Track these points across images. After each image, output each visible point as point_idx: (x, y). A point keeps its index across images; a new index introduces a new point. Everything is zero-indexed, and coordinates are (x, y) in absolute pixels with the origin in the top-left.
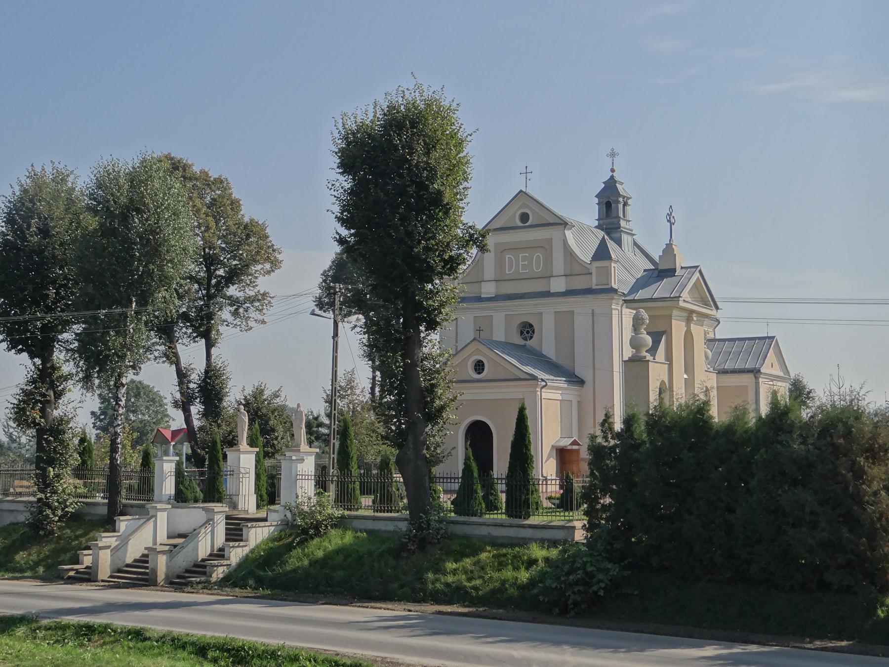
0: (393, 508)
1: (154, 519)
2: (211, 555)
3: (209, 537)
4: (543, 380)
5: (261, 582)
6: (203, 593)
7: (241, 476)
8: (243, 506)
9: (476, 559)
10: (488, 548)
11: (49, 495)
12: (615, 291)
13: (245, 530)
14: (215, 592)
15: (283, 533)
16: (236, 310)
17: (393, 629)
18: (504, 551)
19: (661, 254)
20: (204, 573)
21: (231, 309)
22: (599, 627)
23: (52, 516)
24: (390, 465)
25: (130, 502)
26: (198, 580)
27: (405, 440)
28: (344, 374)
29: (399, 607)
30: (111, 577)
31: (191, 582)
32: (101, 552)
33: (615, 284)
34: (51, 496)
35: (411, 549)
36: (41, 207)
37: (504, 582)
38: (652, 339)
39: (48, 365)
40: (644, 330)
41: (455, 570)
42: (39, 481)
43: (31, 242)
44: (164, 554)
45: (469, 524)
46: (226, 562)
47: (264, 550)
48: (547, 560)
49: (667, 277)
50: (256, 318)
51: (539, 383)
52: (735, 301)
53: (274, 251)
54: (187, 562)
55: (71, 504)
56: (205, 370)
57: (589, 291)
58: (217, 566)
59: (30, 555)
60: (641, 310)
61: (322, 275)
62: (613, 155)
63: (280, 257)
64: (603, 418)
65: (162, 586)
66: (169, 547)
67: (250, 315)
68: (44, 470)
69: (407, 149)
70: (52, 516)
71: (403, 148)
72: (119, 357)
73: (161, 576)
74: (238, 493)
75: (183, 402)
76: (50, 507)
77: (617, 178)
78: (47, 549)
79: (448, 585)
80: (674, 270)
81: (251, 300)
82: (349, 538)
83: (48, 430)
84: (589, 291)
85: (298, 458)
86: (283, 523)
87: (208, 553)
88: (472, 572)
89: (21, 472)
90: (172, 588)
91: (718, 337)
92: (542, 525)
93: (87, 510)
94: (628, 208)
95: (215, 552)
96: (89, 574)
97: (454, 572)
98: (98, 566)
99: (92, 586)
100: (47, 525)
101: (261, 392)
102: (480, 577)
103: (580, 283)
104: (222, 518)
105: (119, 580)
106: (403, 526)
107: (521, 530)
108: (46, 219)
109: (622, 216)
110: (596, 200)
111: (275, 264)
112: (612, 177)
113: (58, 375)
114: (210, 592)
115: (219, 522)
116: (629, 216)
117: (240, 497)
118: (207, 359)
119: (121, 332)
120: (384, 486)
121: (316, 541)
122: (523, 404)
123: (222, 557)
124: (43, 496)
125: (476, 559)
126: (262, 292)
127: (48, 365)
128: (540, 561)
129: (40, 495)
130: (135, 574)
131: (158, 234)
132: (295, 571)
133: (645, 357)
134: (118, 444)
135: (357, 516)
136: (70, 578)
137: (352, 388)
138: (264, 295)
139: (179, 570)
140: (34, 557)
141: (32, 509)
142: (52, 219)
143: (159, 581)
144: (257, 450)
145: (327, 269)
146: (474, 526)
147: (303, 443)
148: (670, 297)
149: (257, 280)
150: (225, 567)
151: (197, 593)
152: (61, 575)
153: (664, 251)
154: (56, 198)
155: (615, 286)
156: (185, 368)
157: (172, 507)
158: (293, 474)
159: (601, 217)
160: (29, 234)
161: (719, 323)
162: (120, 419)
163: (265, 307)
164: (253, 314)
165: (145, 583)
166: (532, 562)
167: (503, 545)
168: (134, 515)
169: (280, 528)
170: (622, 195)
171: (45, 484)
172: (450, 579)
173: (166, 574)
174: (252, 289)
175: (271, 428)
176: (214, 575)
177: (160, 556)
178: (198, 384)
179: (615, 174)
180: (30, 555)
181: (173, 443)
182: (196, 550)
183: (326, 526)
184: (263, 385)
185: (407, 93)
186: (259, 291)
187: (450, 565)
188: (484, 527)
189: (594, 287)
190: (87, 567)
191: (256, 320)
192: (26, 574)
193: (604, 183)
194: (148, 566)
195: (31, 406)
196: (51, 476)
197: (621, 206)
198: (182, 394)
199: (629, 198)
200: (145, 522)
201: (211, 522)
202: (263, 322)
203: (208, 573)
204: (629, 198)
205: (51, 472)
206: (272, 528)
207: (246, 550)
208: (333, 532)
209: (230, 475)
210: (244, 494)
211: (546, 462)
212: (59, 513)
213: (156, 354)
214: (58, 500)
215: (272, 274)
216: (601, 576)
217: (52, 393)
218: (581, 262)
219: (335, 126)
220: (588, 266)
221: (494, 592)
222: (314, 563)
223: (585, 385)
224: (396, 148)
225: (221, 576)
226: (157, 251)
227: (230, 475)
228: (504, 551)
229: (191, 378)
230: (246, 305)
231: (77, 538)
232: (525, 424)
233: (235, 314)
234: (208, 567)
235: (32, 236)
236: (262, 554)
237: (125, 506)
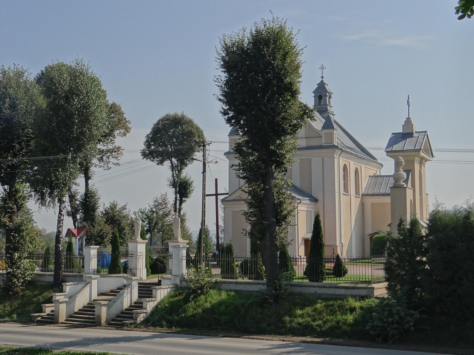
0: (235, 276)
1: (90, 284)
2: (130, 306)
3: (129, 295)
4: (299, 199)
5: (170, 324)
6: (136, 331)
7: (138, 257)
9: (313, 307)
10: (320, 301)
11: (15, 269)
12: (337, 147)
13: (154, 291)
14: (143, 330)
15: (177, 292)
16: (102, 157)
18: (331, 303)
19: (404, 124)
20: (132, 318)
21: (98, 156)
22: (385, 348)
23: (17, 283)
24: (232, 250)
25: (67, 273)
26: (130, 322)
27: (264, 235)
28: (161, 196)
29: (275, 338)
30: (66, 320)
32: (61, 305)
33: (335, 143)
34: (16, 271)
35: (270, 302)
36: (11, 91)
37: (338, 322)
38: (407, 174)
39: (13, 190)
40: (402, 169)
41: (302, 315)
42: (8, 261)
43: (6, 114)
44: (105, 306)
45: (301, 286)
46: (145, 311)
47: (168, 303)
48: (361, 308)
49: (409, 137)
50: (113, 162)
51: (297, 201)
52: (441, 150)
53: (126, 122)
54: (117, 310)
55: (28, 275)
56: (85, 193)
57: (320, 147)
58: (140, 313)
59: (5, 307)
60: (400, 157)
62: (322, 68)
63: (130, 126)
64: (399, 222)
65: (104, 326)
66: (108, 302)
67: (110, 160)
68: (12, 254)
69: (272, 57)
70: (17, 283)
71: (269, 56)
72: (64, 184)
73: (103, 320)
74: (136, 267)
75: (72, 212)
76: (16, 277)
77: (325, 82)
78: (16, 304)
79: (299, 324)
80: (412, 134)
81: (111, 151)
82: (224, 295)
83: (13, 230)
84: (320, 147)
85: (183, 246)
86: (175, 286)
87: (129, 306)
88: (313, 316)
89: (374, 262)
90: (114, 327)
91: (382, 174)
92: (351, 287)
93: (38, 278)
94: (331, 99)
95: (133, 304)
96: (53, 319)
97: (302, 316)
99: (58, 326)
100: (14, 288)
101: (115, 207)
102: (320, 319)
103: (315, 142)
104: (136, 283)
105: (73, 323)
106: (264, 287)
107: (337, 290)
108: (14, 99)
109: (328, 104)
110: (313, 95)
111: (127, 130)
112: (322, 81)
113: (19, 196)
114: (140, 329)
115: (134, 286)
116: (332, 105)
117: (138, 270)
118: (86, 186)
119: (65, 170)
120: (229, 263)
121: (202, 297)
122: (318, 213)
123: (141, 307)
124: (11, 270)
125: (313, 307)
126: (117, 147)
127: (13, 190)
128: (357, 309)
129: (10, 270)
130: (83, 319)
131: (88, 109)
132: (194, 316)
133: (404, 185)
134: (61, 238)
135: (225, 282)
136: (38, 321)
137: (166, 204)
138: (119, 148)
139: (113, 316)
140: (8, 308)
141: (4, 278)
142: (17, 99)
143: (102, 323)
144: (147, 241)
145: (149, 134)
146: (305, 288)
147: (179, 237)
148: (415, 150)
149: (115, 139)
150: (144, 314)
151: (133, 330)
152: (32, 320)
153: (405, 122)
154: (18, 87)
155: (336, 144)
157: (100, 277)
158: (181, 257)
159: (316, 104)
160: (3, 108)
161: (383, 166)
162: (61, 222)
163: (119, 156)
164: (112, 160)
165: (93, 324)
166: (352, 310)
167: (331, 299)
168: (74, 282)
169: (173, 289)
170: (328, 92)
171: (12, 263)
172: (300, 320)
173: (106, 318)
174: (111, 144)
175: (122, 227)
176: (138, 319)
177: (103, 307)
178: (80, 201)
179: (323, 79)
180: (5, 307)
181: (78, 237)
182: (122, 303)
183: (207, 288)
184: (116, 202)
185: (267, 23)
186: (115, 146)
187: (299, 312)
188: (312, 288)
189: (324, 145)
190: (48, 315)
191: (113, 164)
192: (6, 319)
193: (317, 84)
194: (95, 314)
195: (3, 215)
196: (16, 258)
197: (327, 98)
198: (72, 207)
199: (332, 94)
200: (84, 286)
201: (130, 286)
202: (118, 164)
203: (134, 318)
204: (332, 94)
205: (16, 255)
206: (169, 289)
207: (155, 303)
208: (212, 292)
209: (131, 256)
210: (140, 268)
211: (300, 246)
212: (22, 281)
214: (20, 272)
216: (408, 318)
217: (15, 207)
218: (316, 131)
219: (220, 42)
220: (320, 133)
221: (331, 328)
222: (205, 311)
223: (318, 202)
224: (264, 56)
225: (142, 319)
226: (88, 118)
227: (131, 256)
228: (331, 303)
229: (77, 198)
230: (108, 154)
231: (35, 296)
232: (320, 225)
234: (134, 314)
235: (6, 109)
236: (167, 305)
237: (64, 276)
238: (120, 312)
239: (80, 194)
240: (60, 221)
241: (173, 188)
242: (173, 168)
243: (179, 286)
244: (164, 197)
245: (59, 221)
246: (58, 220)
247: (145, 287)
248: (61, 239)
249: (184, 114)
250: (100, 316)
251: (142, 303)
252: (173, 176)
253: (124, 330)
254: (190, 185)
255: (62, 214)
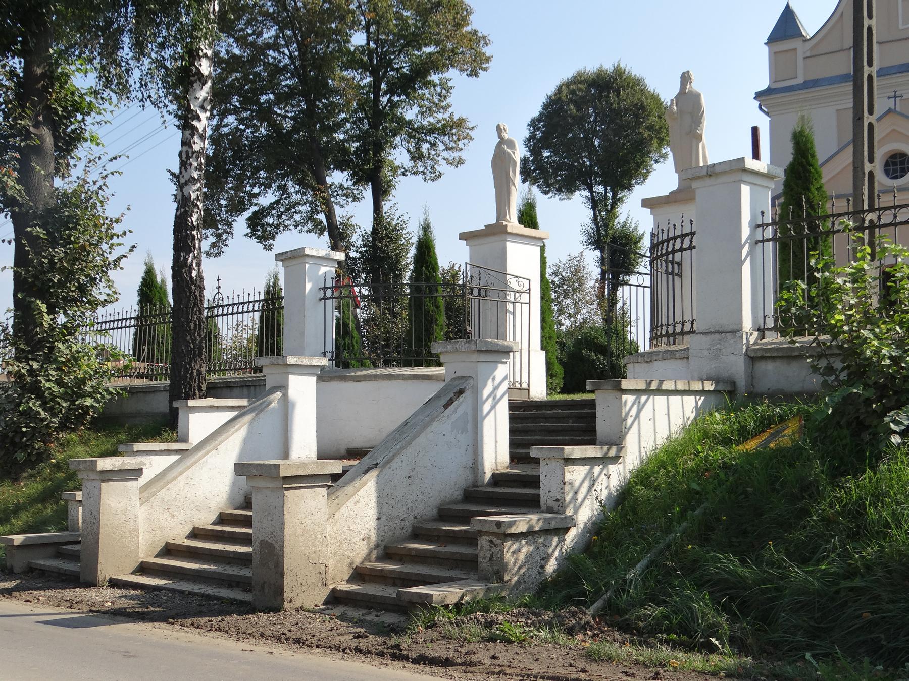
8: (518, 379)
17: (115, 483)
31: (424, 602)
61: (529, 125)
98: (97, 534)
118: (375, 212)
138: (460, 123)
156: (341, 224)
162: (195, 164)
203: (484, 564)
213: (297, 217)
215: (449, 166)
233: (416, 156)
234: (483, 541)
238: (408, 526)
239: (358, 230)
240: (188, 158)
241: (595, 249)
242: (595, 203)
243: (742, 384)
244: (576, 263)
245: (184, 158)
246: (180, 155)
247: (546, 418)
248: (194, 232)
249: (622, 66)
250: (277, 547)
251: (534, 482)
252: (595, 220)
253: (406, 658)
254: (636, 243)
255: (194, 129)
